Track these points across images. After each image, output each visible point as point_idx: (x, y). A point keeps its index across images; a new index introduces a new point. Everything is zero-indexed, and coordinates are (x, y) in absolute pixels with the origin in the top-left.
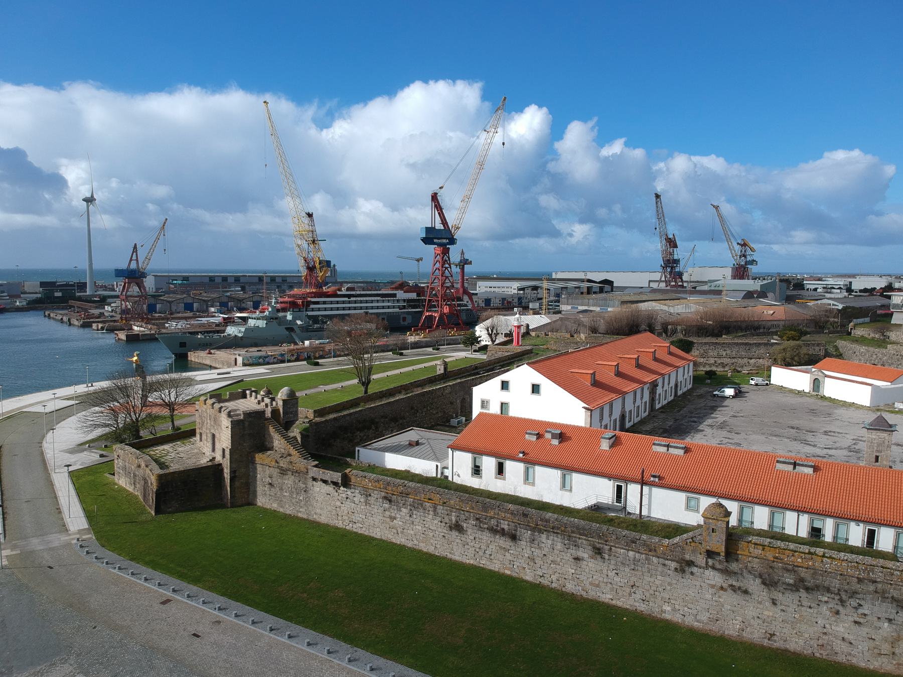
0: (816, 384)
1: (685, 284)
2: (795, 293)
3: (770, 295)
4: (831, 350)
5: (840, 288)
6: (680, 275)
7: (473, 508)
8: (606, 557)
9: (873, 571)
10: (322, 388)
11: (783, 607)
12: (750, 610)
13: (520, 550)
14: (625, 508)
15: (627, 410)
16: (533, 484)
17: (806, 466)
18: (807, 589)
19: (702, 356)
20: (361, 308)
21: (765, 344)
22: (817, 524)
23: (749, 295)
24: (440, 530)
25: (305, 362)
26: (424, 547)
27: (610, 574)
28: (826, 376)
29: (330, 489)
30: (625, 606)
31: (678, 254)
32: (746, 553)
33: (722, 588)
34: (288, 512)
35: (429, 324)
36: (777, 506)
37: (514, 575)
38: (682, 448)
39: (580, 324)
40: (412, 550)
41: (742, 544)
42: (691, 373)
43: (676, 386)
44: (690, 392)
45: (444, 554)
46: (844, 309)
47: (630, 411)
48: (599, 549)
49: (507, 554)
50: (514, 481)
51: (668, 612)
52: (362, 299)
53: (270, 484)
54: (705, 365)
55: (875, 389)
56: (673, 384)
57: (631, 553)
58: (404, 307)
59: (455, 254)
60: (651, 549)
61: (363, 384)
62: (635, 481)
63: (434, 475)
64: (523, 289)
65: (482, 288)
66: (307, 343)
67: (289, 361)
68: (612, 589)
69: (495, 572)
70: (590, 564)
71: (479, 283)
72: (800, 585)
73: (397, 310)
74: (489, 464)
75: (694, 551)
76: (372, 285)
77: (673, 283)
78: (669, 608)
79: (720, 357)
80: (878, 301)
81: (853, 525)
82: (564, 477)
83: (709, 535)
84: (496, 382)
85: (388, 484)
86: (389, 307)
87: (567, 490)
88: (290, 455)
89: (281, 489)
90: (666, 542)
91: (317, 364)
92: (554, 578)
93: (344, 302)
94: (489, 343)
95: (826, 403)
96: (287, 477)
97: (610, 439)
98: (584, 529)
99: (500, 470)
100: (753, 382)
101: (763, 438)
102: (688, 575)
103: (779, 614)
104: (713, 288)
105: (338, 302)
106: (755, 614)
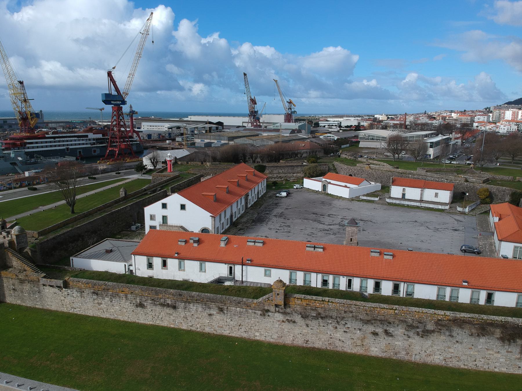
0: (324, 187)
1: (261, 124)
2: (315, 129)
3: (303, 131)
4: (331, 166)
5: (336, 126)
6: (258, 119)
7: (150, 294)
8: (226, 312)
9: (351, 307)
10: (41, 208)
11: (312, 327)
12: (297, 330)
13: (178, 313)
14: (234, 278)
15: (234, 212)
16: (184, 270)
17: (320, 248)
18: (322, 318)
19: (270, 173)
20: (64, 145)
21: (301, 166)
22: (325, 278)
23: (293, 131)
24: (130, 308)
25: (26, 188)
26: (121, 318)
27: (228, 320)
28: (330, 183)
29: (56, 290)
30: (236, 336)
31: (257, 107)
32: (294, 303)
33: (283, 321)
34: (29, 305)
35: (112, 155)
36: (307, 271)
37: (176, 327)
38: (262, 243)
39: (206, 155)
40: (114, 321)
41: (292, 299)
42: (265, 185)
43: (258, 193)
44: (265, 194)
45: (134, 320)
46: (338, 139)
47: (235, 212)
48: (221, 309)
49: (171, 316)
50: (173, 271)
51: (258, 336)
52: (64, 139)
53: (14, 289)
54: (272, 178)
55: (351, 189)
56: (256, 192)
57: (238, 309)
58: (94, 144)
59: (126, 109)
60: (248, 306)
61: (70, 205)
62: (238, 264)
63: (124, 273)
64: (171, 128)
65: (146, 127)
66: (27, 174)
67: (15, 188)
68: (229, 328)
69: (165, 327)
70: (217, 317)
71: (143, 124)
72: (319, 316)
73: (89, 146)
74: (157, 261)
75: (269, 305)
76: (70, 126)
77: (255, 124)
78: (258, 334)
79: (279, 173)
80: (353, 134)
81: (341, 277)
82: (201, 265)
83: (276, 297)
84: (159, 204)
85: (95, 285)
86: (83, 144)
87: (203, 272)
88: (25, 270)
89: (22, 292)
90: (255, 301)
91: (35, 189)
92: (198, 326)
93: (51, 142)
94: (153, 168)
95: (329, 198)
96: (25, 284)
97: (225, 241)
98: (213, 299)
99: (164, 264)
100: (295, 187)
101: (300, 221)
102: (267, 317)
103: (310, 331)
104: (275, 128)
105: (46, 142)
106: (299, 332)
